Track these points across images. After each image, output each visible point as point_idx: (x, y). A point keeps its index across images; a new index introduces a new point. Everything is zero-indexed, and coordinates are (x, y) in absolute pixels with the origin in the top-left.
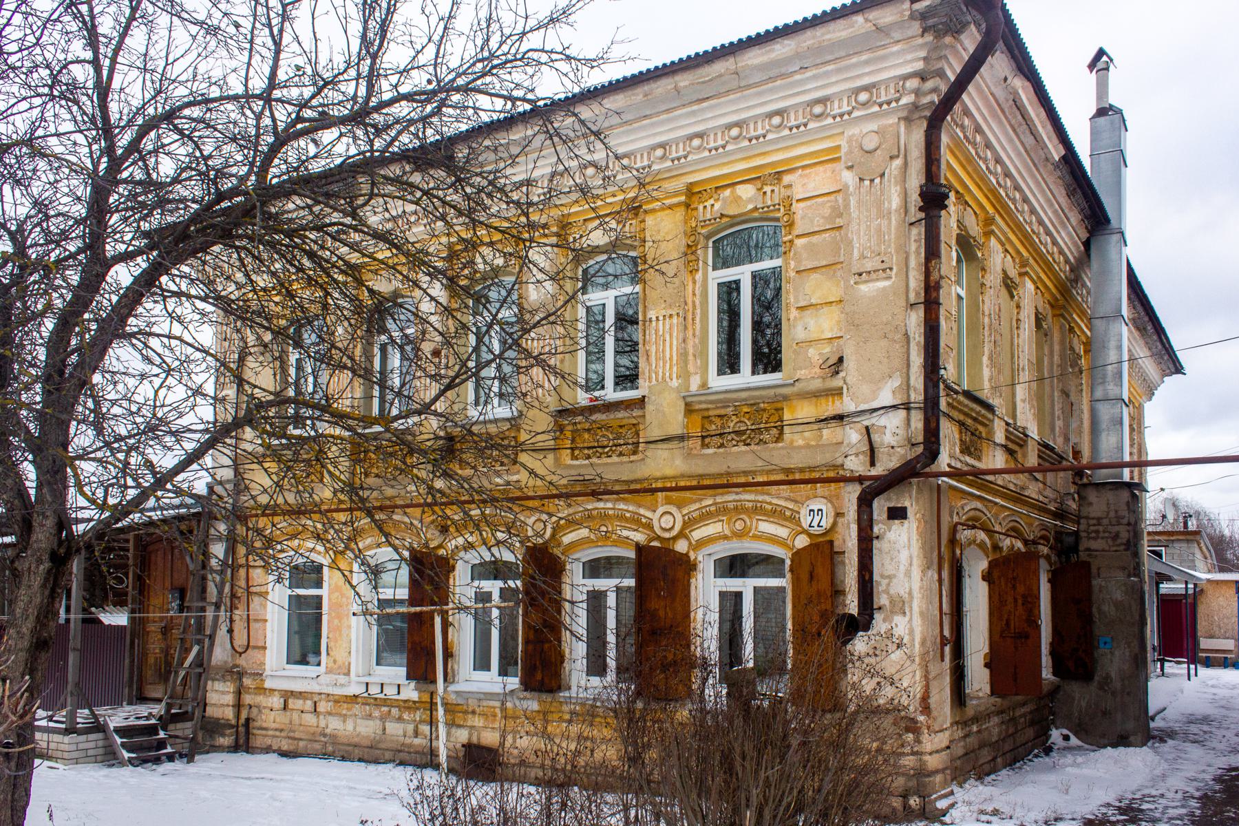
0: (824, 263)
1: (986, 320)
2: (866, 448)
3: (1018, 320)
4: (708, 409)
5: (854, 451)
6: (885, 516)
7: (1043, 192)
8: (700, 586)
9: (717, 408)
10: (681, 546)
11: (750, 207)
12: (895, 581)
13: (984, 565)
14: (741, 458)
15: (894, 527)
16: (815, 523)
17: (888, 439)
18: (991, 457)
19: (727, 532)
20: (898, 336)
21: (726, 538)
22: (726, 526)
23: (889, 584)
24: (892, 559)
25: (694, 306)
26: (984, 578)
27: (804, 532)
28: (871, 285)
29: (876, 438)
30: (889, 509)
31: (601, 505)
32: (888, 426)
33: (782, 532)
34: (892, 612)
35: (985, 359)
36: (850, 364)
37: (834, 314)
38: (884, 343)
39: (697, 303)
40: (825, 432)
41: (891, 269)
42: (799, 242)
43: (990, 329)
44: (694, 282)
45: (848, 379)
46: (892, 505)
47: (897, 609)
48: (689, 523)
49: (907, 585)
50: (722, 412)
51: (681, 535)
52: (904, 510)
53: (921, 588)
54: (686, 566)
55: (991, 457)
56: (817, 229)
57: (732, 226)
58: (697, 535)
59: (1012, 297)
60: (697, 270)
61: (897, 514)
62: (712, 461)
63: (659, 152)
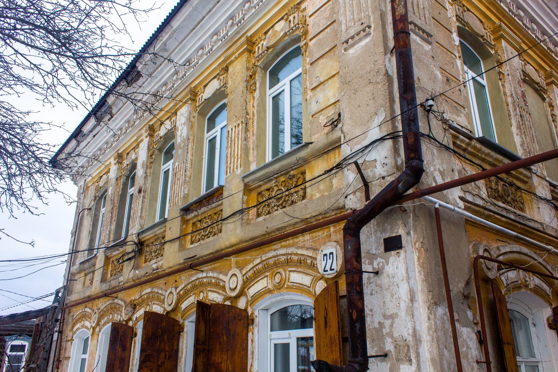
0: (328, 49)
1: (509, 100)
2: (361, 184)
3: (553, 115)
4: (260, 186)
5: (351, 189)
6: (382, 248)
7: (548, 15)
8: (256, 339)
9: (266, 183)
10: (241, 304)
11: (282, 34)
12: (397, 321)
13: (548, 312)
14: (279, 219)
15: (391, 259)
16: (328, 268)
17: (380, 171)
18: (536, 210)
19: (270, 286)
20: (380, 77)
21: (270, 291)
22: (269, 281)
23: (391, 326)
24: (392, 295)
25: (253, 114)
26: (551, 327)
27: (322, 278)
28: (356, 47)
29: (368, 173)
30: (385, 240)
31: (200, 275)
32: (378, 158)
33: (306, 280)
34: (398, 360)
35: (514, 129)
36: (345, 117)
37: (336, 83)
38: (370, 88)
39: (255, 111)
40: (335, 181)
41: (369, 27)
42: (311, 44)
43: (514, 105)
44: (254, 98)
45: (344, 129)
46: (387, 235)
47: (402, 355)
48: (247, 283)
49: (410, 325)
50: (268, 186)
51: (242, 293)
52: (398, 239)
53: (429, 329)
54: (246, 320)
55: (536, 210)
56: (322, 29)
57: (278, 55)
58: (252, 291)
59: (544, 99)
60: (255, 90)
61: (393, 244)
62: (262, 225)
63: (230, 22)
